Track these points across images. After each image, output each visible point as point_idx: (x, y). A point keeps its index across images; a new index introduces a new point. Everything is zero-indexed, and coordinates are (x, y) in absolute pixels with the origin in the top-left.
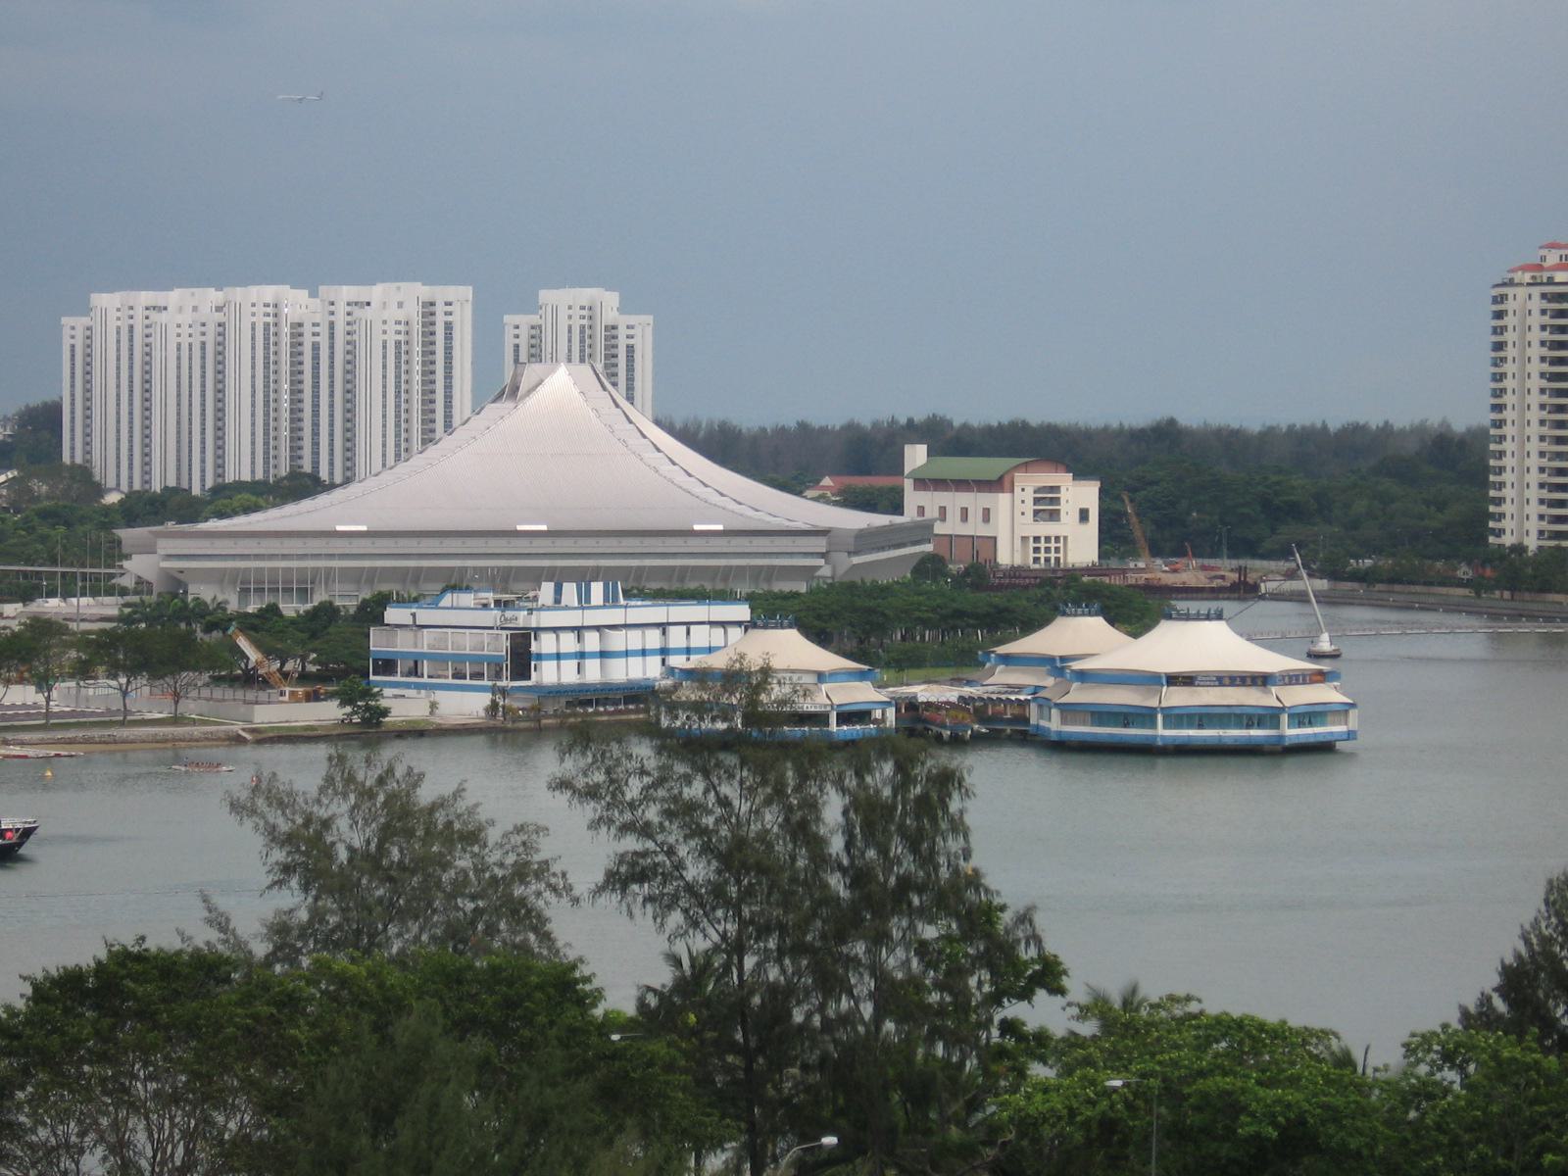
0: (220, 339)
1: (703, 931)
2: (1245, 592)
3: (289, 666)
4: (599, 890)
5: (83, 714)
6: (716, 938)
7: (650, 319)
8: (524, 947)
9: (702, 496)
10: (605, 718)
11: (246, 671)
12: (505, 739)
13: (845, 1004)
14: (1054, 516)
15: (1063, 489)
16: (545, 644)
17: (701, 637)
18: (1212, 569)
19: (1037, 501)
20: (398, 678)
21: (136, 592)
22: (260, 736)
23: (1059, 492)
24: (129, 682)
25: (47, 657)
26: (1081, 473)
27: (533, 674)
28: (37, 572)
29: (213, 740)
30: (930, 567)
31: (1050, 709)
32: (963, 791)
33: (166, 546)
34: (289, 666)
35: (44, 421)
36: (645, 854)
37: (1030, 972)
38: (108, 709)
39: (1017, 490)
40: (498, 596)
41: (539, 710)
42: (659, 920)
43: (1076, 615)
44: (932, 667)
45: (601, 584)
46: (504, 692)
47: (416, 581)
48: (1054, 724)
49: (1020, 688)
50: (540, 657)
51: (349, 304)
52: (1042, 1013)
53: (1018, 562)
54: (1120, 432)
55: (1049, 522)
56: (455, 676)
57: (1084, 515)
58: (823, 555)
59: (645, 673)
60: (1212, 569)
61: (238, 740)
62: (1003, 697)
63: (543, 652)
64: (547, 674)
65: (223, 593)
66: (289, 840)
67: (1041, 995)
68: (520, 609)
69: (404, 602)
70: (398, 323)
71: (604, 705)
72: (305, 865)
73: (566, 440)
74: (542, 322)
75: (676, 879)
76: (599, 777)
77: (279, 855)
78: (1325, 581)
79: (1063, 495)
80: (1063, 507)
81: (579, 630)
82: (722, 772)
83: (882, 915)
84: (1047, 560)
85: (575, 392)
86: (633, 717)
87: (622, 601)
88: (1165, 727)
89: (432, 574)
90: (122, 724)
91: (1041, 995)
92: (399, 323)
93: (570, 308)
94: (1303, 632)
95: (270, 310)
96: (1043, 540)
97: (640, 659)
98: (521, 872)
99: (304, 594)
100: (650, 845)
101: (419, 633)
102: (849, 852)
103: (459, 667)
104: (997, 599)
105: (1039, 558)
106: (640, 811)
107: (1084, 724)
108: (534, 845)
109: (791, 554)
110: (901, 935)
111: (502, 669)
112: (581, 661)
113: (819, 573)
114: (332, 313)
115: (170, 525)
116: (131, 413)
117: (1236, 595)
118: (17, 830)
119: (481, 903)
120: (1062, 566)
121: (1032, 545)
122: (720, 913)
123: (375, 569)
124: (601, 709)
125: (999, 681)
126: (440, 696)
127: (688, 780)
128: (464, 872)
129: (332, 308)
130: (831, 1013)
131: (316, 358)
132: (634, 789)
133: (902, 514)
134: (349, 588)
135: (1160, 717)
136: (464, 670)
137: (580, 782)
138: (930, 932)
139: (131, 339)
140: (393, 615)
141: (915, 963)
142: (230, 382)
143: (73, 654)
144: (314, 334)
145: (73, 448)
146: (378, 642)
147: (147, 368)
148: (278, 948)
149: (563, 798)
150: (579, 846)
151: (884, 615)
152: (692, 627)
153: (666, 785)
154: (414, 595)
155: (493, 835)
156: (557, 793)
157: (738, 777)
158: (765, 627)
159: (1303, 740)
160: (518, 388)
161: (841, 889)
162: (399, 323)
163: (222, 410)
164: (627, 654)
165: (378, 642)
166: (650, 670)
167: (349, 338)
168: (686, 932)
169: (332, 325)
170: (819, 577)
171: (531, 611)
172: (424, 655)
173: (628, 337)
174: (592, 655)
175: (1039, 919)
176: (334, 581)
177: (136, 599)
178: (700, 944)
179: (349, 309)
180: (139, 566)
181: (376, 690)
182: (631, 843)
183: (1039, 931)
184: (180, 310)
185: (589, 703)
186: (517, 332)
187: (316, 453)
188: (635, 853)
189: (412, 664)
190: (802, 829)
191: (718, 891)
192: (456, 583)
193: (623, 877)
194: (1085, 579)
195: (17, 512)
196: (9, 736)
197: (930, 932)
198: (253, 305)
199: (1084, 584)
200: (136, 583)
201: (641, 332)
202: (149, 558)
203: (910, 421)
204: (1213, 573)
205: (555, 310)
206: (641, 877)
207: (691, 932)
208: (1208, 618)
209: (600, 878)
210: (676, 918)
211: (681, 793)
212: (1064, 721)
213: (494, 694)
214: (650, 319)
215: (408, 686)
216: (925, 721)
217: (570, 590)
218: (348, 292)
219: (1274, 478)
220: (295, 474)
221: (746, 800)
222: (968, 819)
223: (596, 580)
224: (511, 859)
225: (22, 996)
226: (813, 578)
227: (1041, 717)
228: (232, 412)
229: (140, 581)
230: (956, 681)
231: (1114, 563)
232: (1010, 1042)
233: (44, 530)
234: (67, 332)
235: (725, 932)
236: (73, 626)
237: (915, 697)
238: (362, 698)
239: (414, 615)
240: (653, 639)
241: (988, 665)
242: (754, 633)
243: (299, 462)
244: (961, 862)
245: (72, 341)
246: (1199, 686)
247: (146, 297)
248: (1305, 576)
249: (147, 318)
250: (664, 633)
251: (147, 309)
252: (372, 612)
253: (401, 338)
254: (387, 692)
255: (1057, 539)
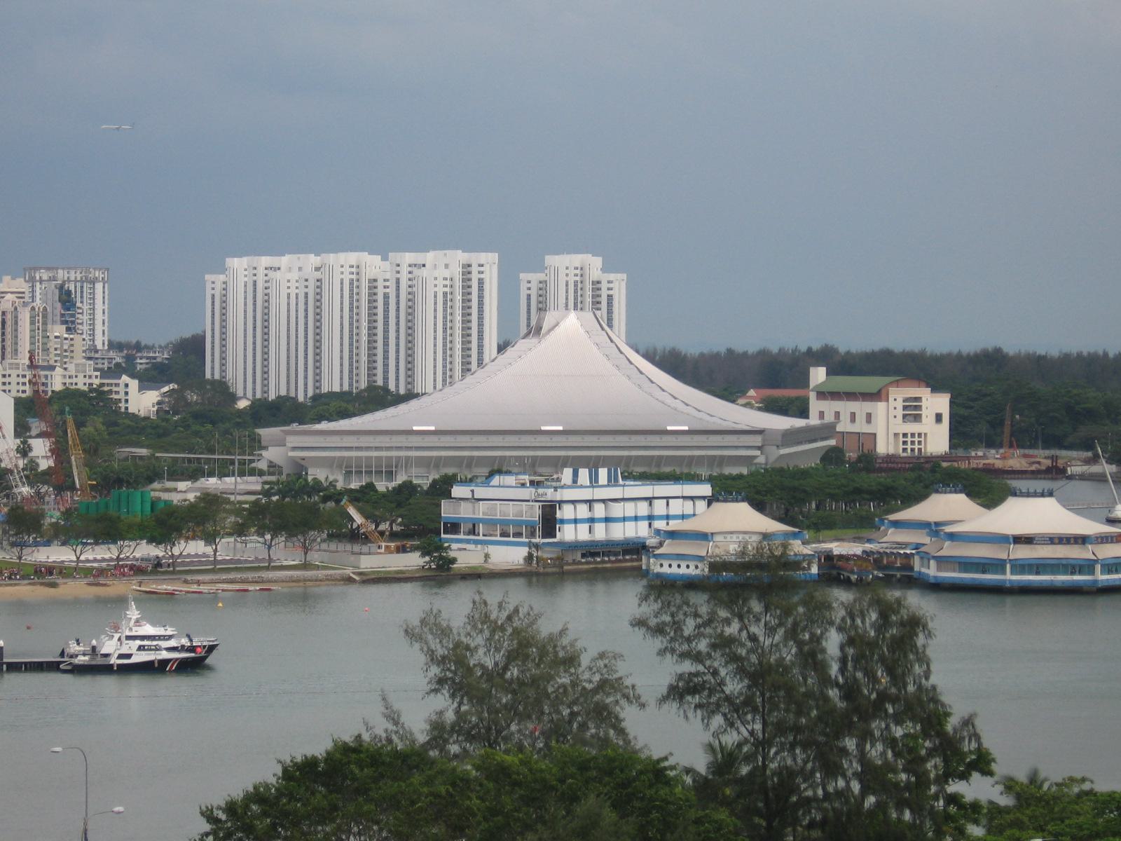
0: (318, 290)
1: (737, 729)
2: (1056, 473)
3: (383, 527)
4: (664, 699)
5: (239, 561)
6: (746, 733)
7: (624, 276)
8: (605, 742)
9: (673, 405)
10: (608, 565)
11: (352, 531)
12: (538, 581)
13: (841, 783)
14: (917, 418)
15: (924, 399)
16: (566, 512)
17: (676, 507)
18: (1032, 456)
19: (905, 408)
20: (461, 536)
21: (270, 474)
22: (365, 578)
23: (921, 402)
24: (272, 540)
25: (215, 521)
26: (936, 389)
27: (558, 534)
28: (198, 459)
29: (333, 580)
30: (832, 456)
31: (929, 560)
32: (926, 632)
33: (292, 441)
34: (383, 527)
35: (193, 348)
36: (697, 674)
37: (968, 760)
38: (256, 558)
39: (891, 399)
40: (533, 478)
41: (562, 559)
42: (706, 721)
43: (945, 493)
44: (840, 528)
45: (606, 469)
46: (537, 546)
47: (469, 466)
48: (932, 571)
49: (906, 545)
50: (562, 521)
51: (410, 266)
52: (976, 789)
53: (891, 451)
54: (959, 356)
55: (912, 423)
56: (502, 535)
57: (939, 418)
58: (759, 448)
59: (637, 533)
60: (1032, 456)
61: (349, 580)
62: (895, 551)
63: (565, 518)
64: (567, 534)
65: (333, 475)
66: (443, 661)
67: (976, 776)
68: (548, 487)
69: (466, 482)
70: (445, 279)
71: (608, 556)
72: (453, 680)
73: (575, 364)
74: (547, 278)
75: (719, 692)
76: (667, 618)
77: (435, 670)
78: (1114, 466)
79: (924, 403)
80: (924, 412)
81: (590, 502)
82: (751, 616)
83: (866, 717)
84: (913, 450)
85: (582, 331)
86: (629, 564)
87: (621, 482)
88: (1012, 573)
89: (481, 461)
90: (267, 568)
91: (976, 776)
92: (446, 279)
93: (567, 268)
94: (1108, 504)
95: (354, 270)
96: (909, 435)
97: (633, 523)
98: (603, 685)
99: (390, 475)
100: (701, 668)
101: (476, 505)
102: (843, 675)
103: (505, 528)
104: (883, 478)
105: (906, 449)
106: (694, 643)
107: (954, 571)
108: (614, 668)
109: (737, 447)
110: (879, 733)
111: (535, 530)
112: (592, 524)
113: (757, 461)
114: (398, 272)
115: (295, 426)
116: (254, 343)
117: (1050, 476)
118: (204, 647)
119: (575, 709)
120: (923, 454)
121: (901, 439)
122: (749, 717)
123: (440, 457)
124: (606, 559)
125: (890, 539)
126: (492, 549)
127: (727, 622)
128: (564, 686)
129: (398, 269)
130: (831, 789)
131: (386, 304)
132: (689, 626)
133: (807, 417)
134: (422, 471)
135: (1008, 566)
136: (508, 531)
137: (653, 622)
138: (898, 732)
139: (255, 291)
140: (457, 491)
141: (890, 754)
142: (325, 321)
143: (232, 519)
144: (385, 287)
145: (213, 368)
146: (447, 510)
147: (266, 311)
148: (434, 739)
149: (640, 632)
150: (648, 668)
151: (805, 491)
152: (671, 501)
153: (713, 625)
154: (469, 476)
155: (585, 660)
156: (636, 629)
157: (763, 620)
158: (725, 501)
159: (1111, 583)
160: (541, 328)
161: (837, 699)
162: (446, 279)
163: (319, 341)
164: (624, 519)
165: (447, 510)
166: (641, 531)
167: (410, 290)
168: (725, 730)
169: (398, 281)
170: (756, 464)
171: (556, 489)
172: (481, 520)
173: (479, 272)
174: (600, 520)
175: (977, 722)
176: (411, 466)
177: (273, 478)
178: (730, 739)
179: (410, 269)
180: (272, 454)
181: (446, 545)
182: (688, 667)
183: (978, 731)
184: (290, 269)
185: (597, 554)
186: (529, 285)
187: (386, 372)
188: (690, 674)
189: (471, 526)
190: (811, 657)
191: (748, 702)
192: (498, 469)
193: (681, 691)
194: (945, 464)
195: (175, 413)
196: (189, 578)
197: (898, 732)
198: (342, 266)
199: (945, 469)
200: (268, 467)
201: (618, 285)
202: (280, 447)
203: (810, 350)
204: (1033, 460)
205: (557, 271)
206: (694, 690)
207: (729, 729)
208: (1042, 495)
209: (664, 691)
210: (718, 720)
211: (722, 631)
212: (939, 569)
213: (530, 548)
214: (624, 276)
215: (468, 542)
216: (840, 568)
217: (584, 474)
218: (409, 257)
219: (1075, 391)
220: (371, 387)
221: (769, 636)
222: (929, 652)
223: (603, 466)
224: (597, 678)
225: (274, 775)
226: (752, 464)
227: (922, 566)
228: (274, 331)
229: (271, 465)
230: (858, 539)
231: (960, 452)
232: (952, 809)
233: (196, 427)
234: (209, 286)
235: (753, 730)
236: (232, 498)
237: (831, 551)
238: (436, 551)
239: (473, 491)
240: (643, 509)
241: (882, 528)
242: (715, 505)
243: (374, 378)
244: (923, 681)
245: (213, 292)
246: (1036, 544)
247: (265, 261)
248: (1104, 462)
249: (266, 275)
250: (650, 504)
251: (266, 269)
252: (442, 488)
253: (448, 290)
254: (454, 546)
255: (920, 435)
